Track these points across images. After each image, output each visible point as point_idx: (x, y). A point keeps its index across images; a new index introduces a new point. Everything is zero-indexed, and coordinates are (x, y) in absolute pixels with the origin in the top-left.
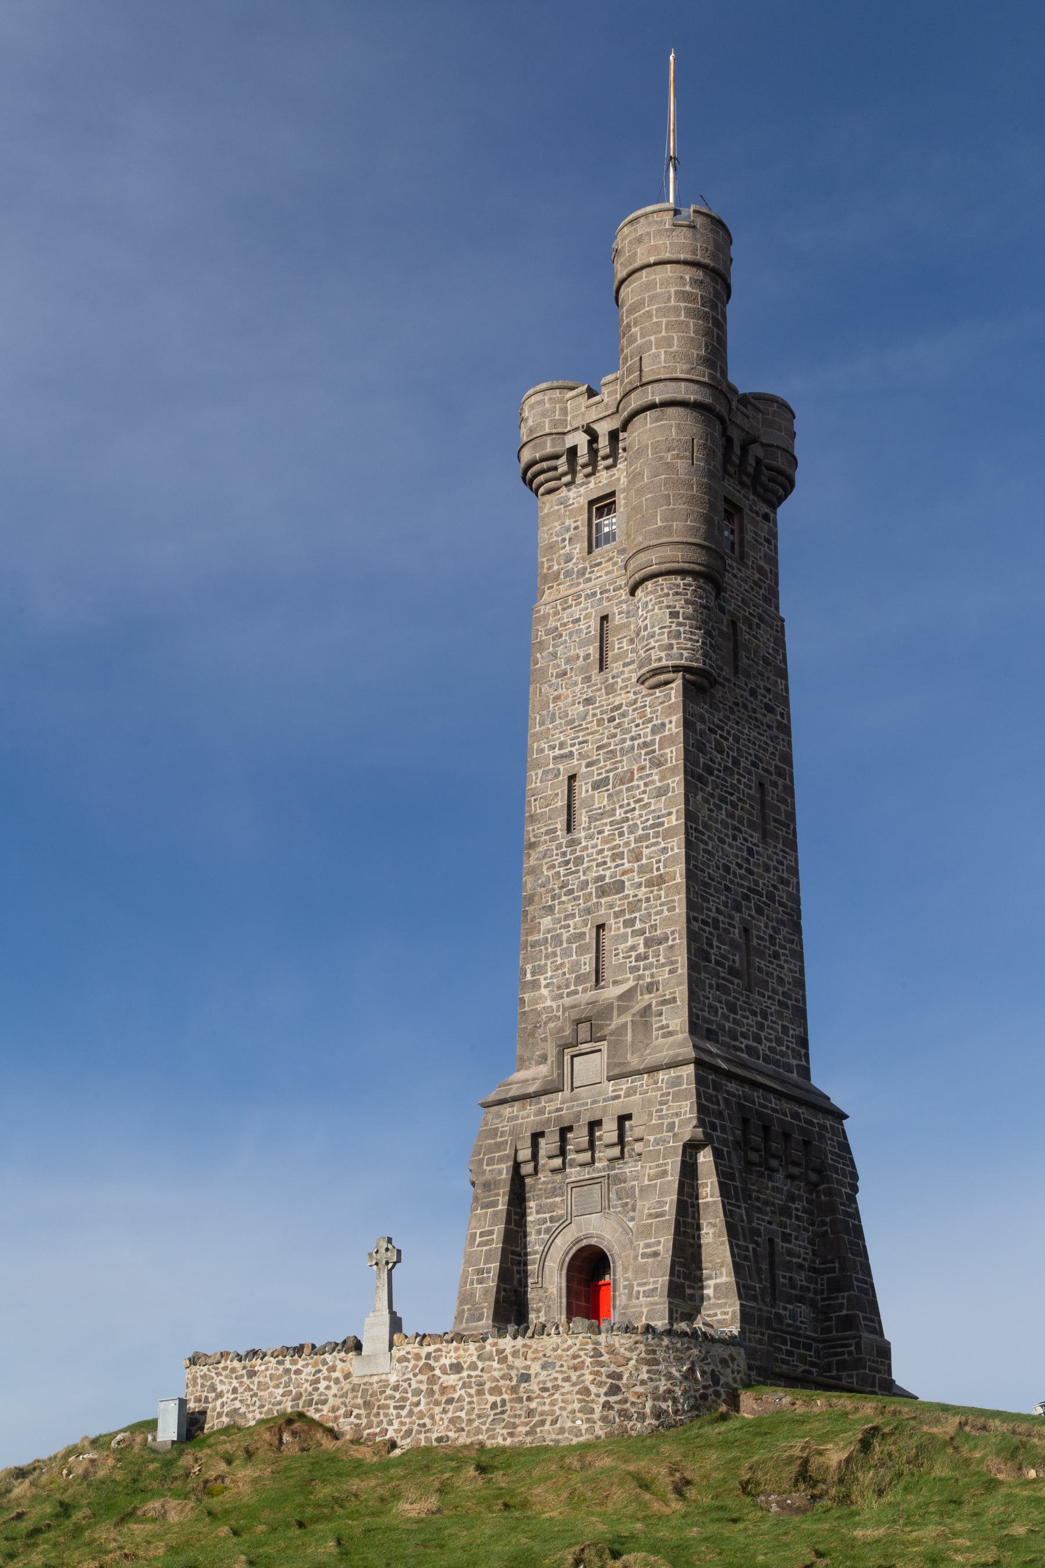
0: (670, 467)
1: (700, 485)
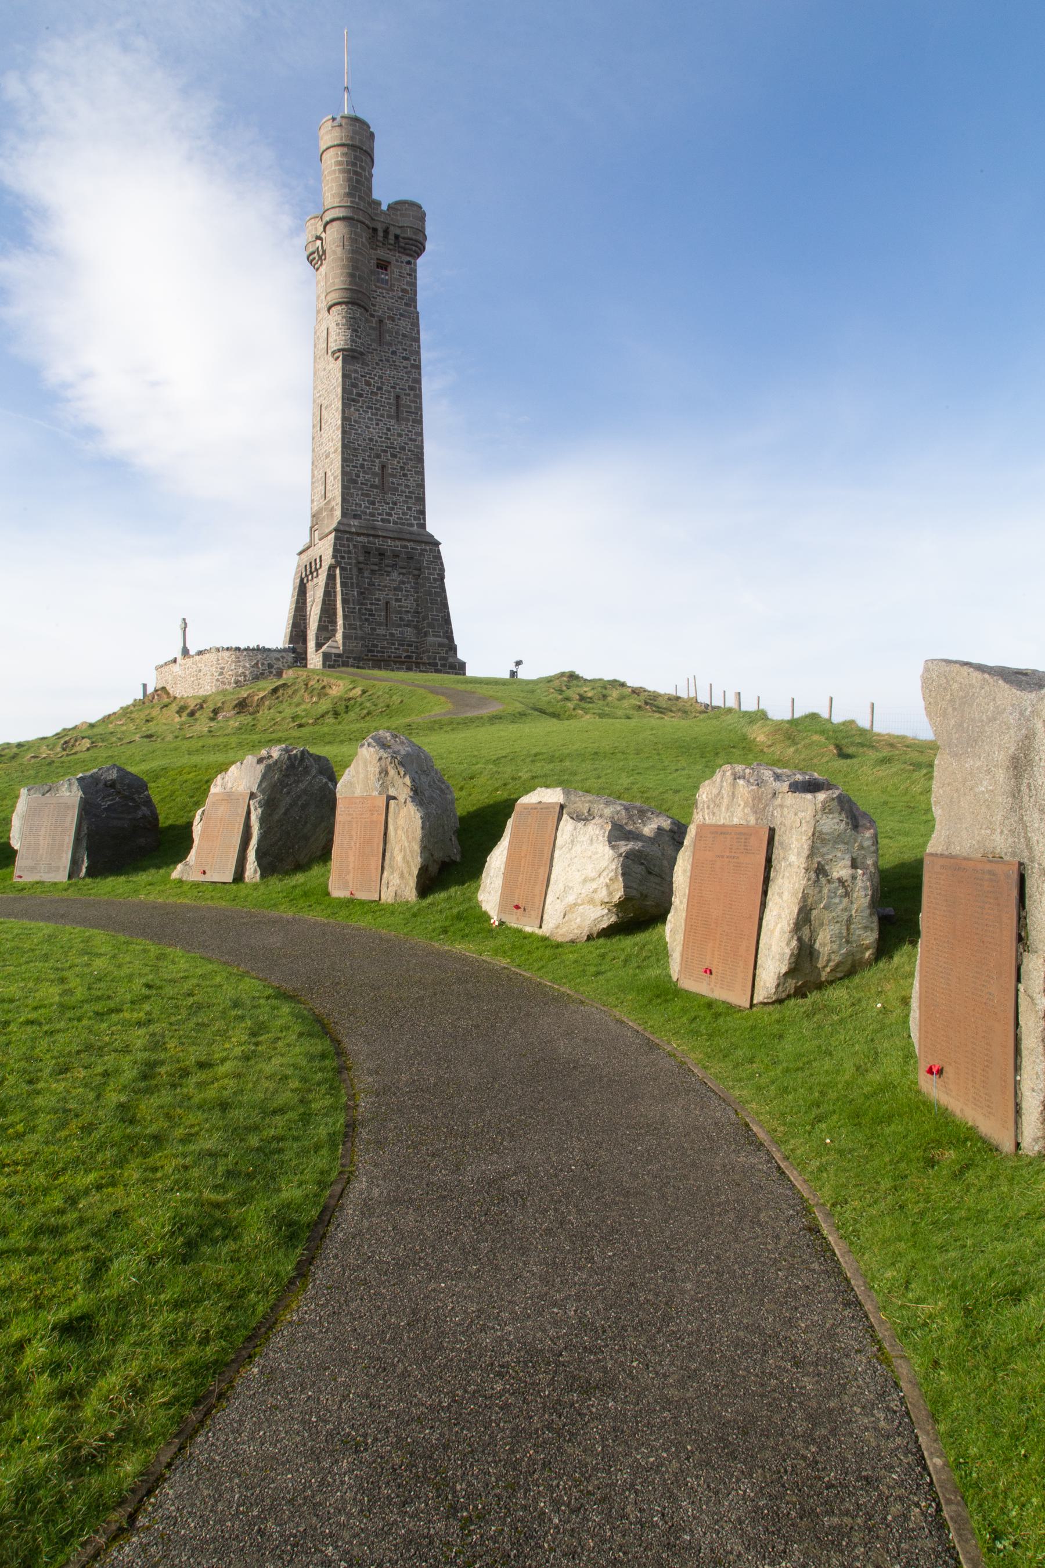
1: (347, 259)
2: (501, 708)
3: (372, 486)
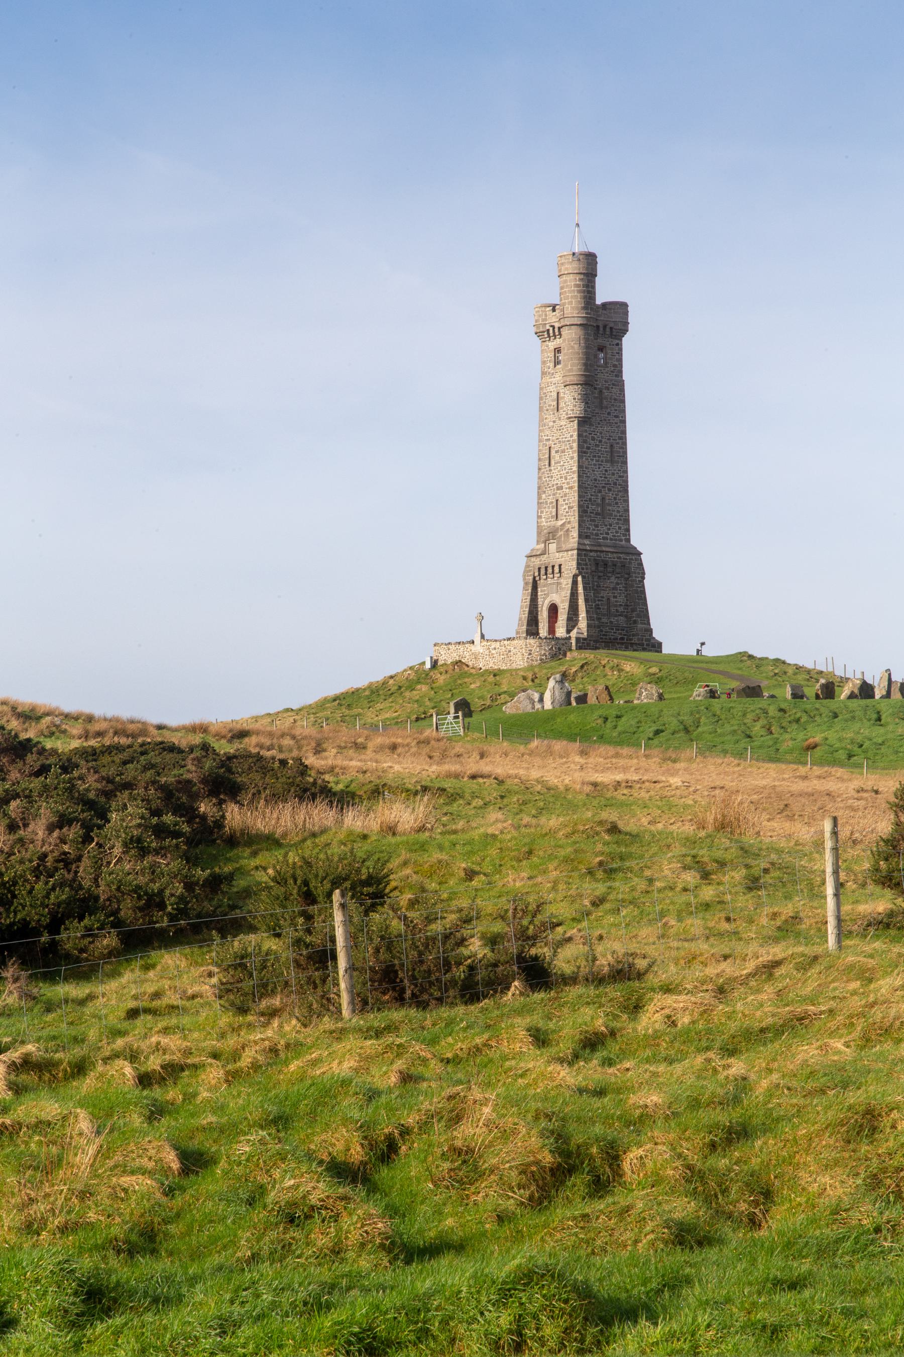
0: (573, 347)
3: (597, 514)
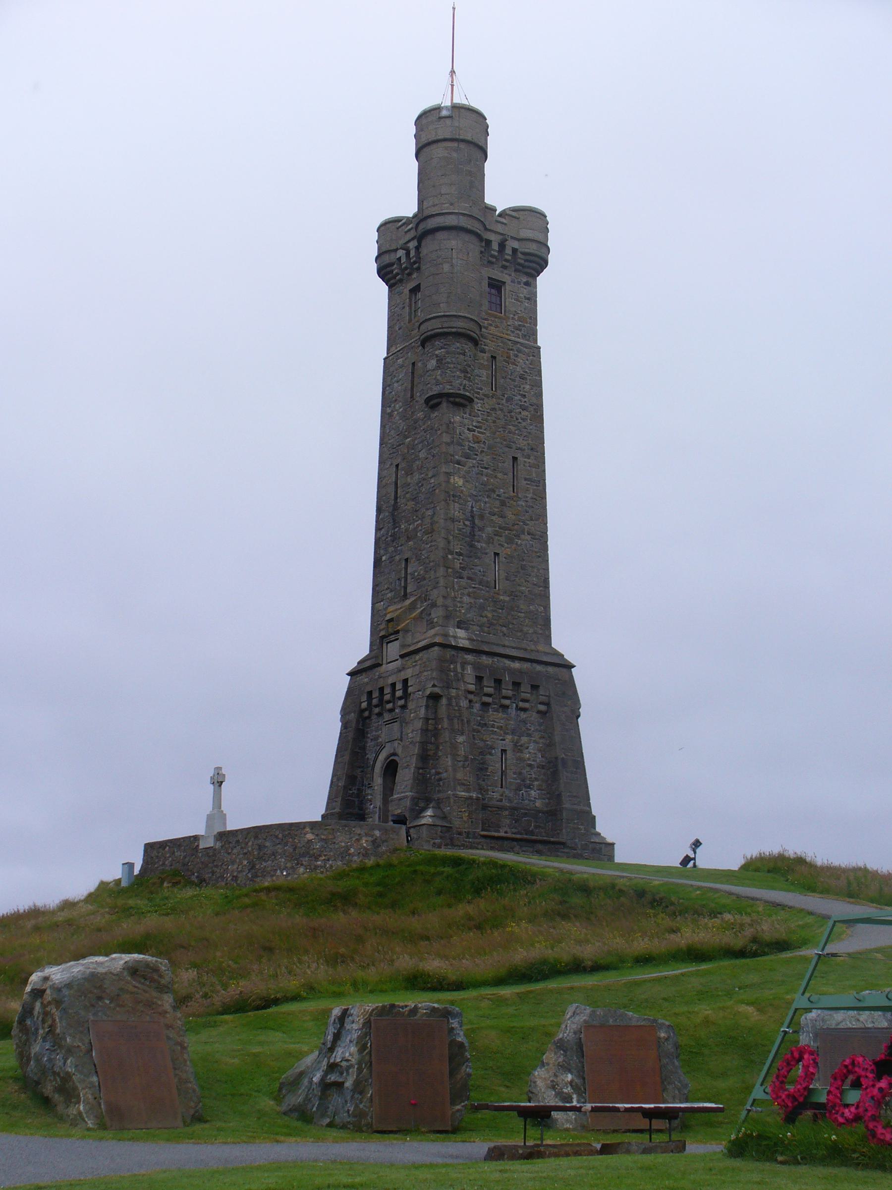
2: (466, 656)
